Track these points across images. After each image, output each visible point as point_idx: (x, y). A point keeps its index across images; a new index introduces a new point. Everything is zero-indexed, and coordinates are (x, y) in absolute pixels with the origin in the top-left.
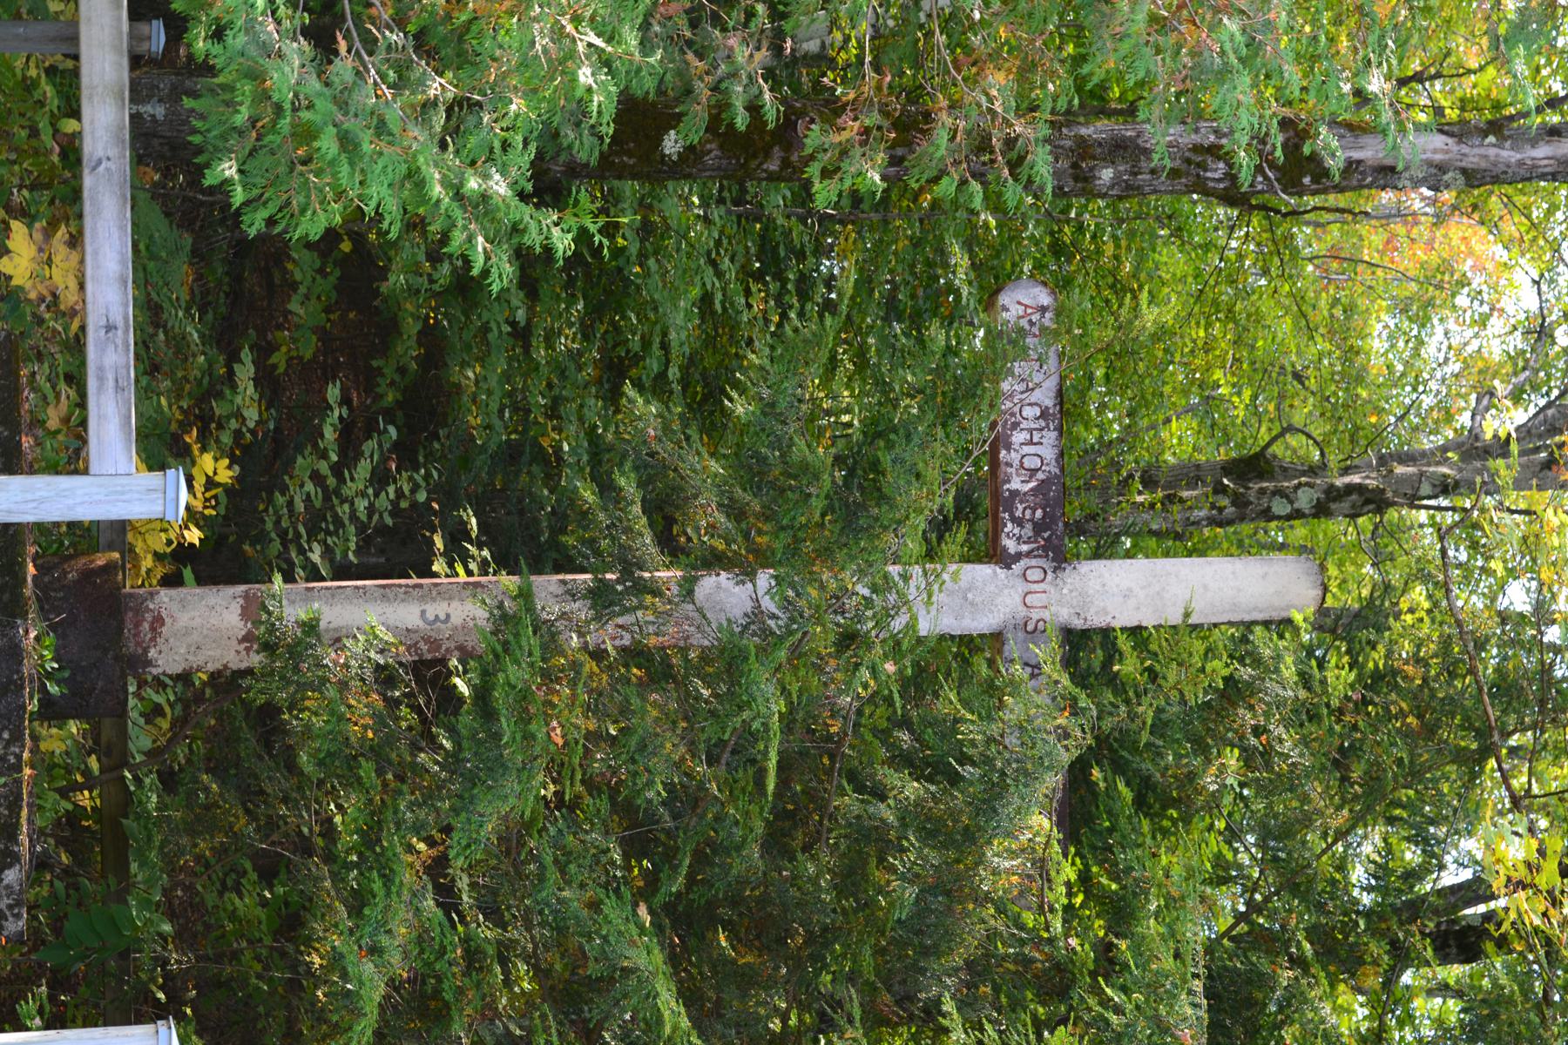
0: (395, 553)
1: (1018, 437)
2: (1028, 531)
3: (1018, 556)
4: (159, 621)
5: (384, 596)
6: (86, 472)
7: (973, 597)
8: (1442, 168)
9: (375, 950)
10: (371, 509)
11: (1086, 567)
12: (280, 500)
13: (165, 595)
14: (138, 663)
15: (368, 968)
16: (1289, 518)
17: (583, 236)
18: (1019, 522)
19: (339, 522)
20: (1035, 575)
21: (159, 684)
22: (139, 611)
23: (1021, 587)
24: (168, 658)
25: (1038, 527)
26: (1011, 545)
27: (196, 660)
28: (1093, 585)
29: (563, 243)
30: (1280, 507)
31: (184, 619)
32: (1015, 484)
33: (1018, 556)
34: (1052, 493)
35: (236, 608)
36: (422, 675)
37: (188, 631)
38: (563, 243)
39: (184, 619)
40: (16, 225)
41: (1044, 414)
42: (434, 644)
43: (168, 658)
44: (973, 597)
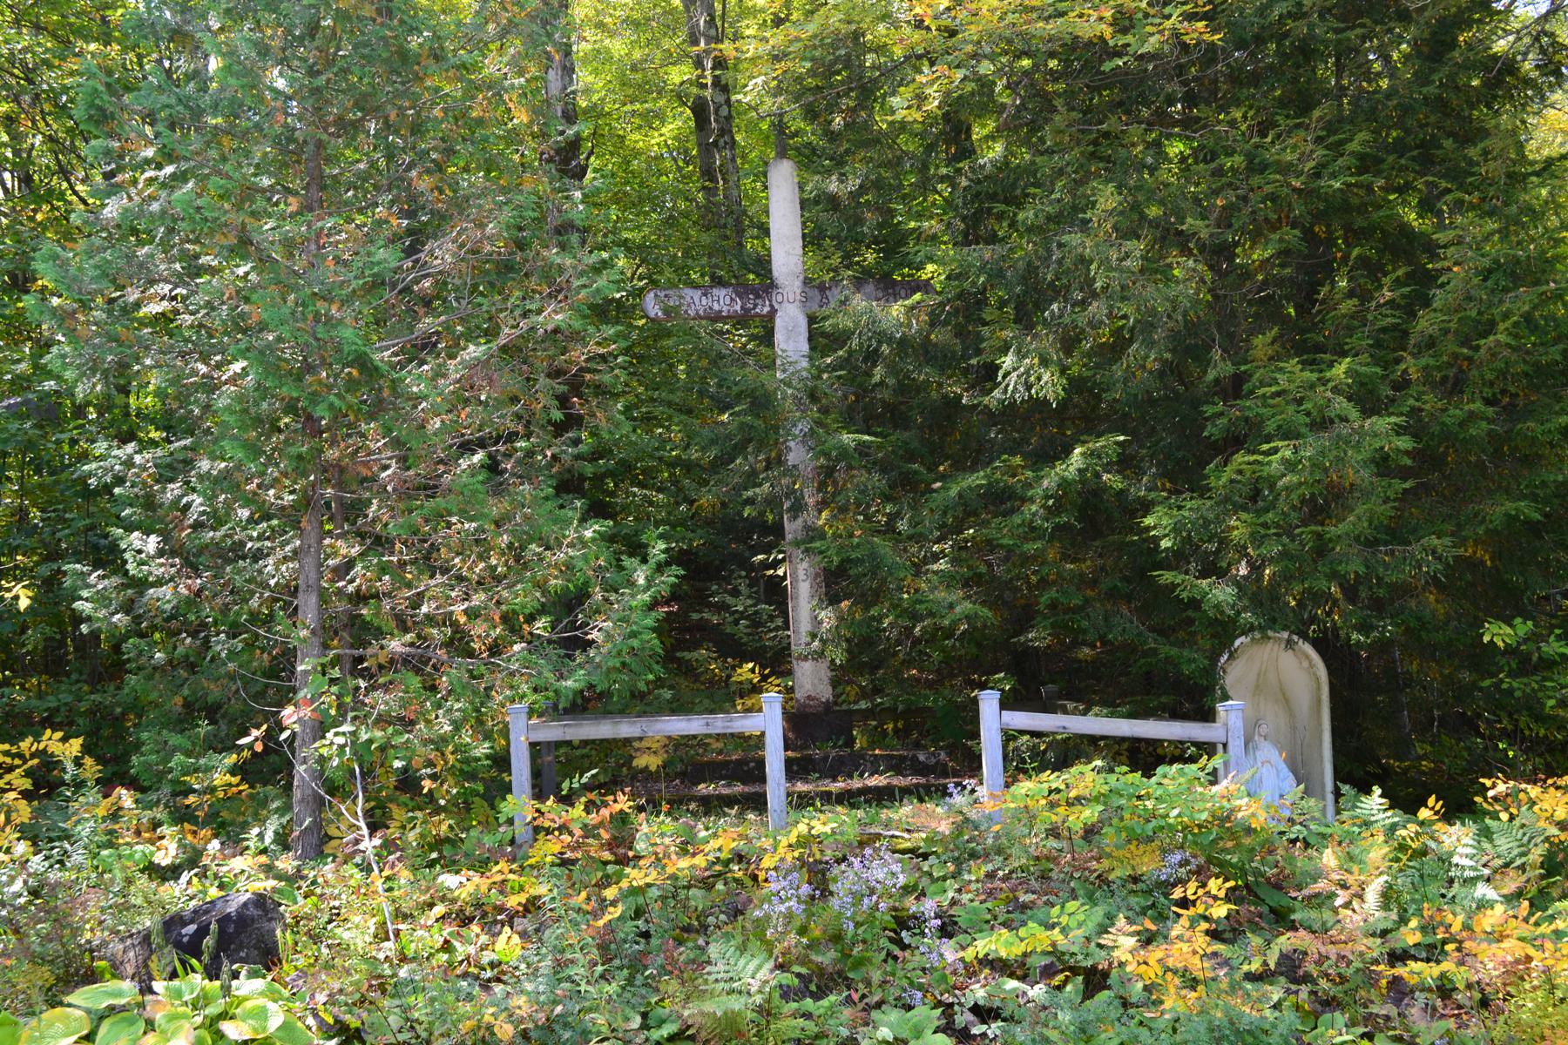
0: (776, 593)
1: (716, 307)
2: (759, 301)
3: (771, 306)
4: (809, 697)
5: (796, 598)
6: (763, 734)
7: (791, 339)
8: (564, 68)
9: (951, 606)
10: (749, 597)
11: (775, 274)
12: (745, 639)
13: (798, 695)
14: (827, 706)
15: (958, 609)
16: (729, 106)
17: (661, 536)
18: (756, 306)
19: (756, 613)
20: (780, 298)
21: (836, 696)
22: (805, 706)
23: (786, 304)
24: (826, 693)
25: (758, 296)
26: (767, 309)
27: (826, 681)
28: (784, 269)
29: (662, 545)
30: (724, 111)
31: (808, 686)
32: (738, 308)
33: (771, 306)
34: (743, 290)
35: (803, 664)
36: (834, 584)
37: (813, 684)
38: (662, 545)
39: (808, 686)
40: (635, 763)
41: (705, 295)
42: (817, 575)
43: (826, 693)
44: (791, 339)
